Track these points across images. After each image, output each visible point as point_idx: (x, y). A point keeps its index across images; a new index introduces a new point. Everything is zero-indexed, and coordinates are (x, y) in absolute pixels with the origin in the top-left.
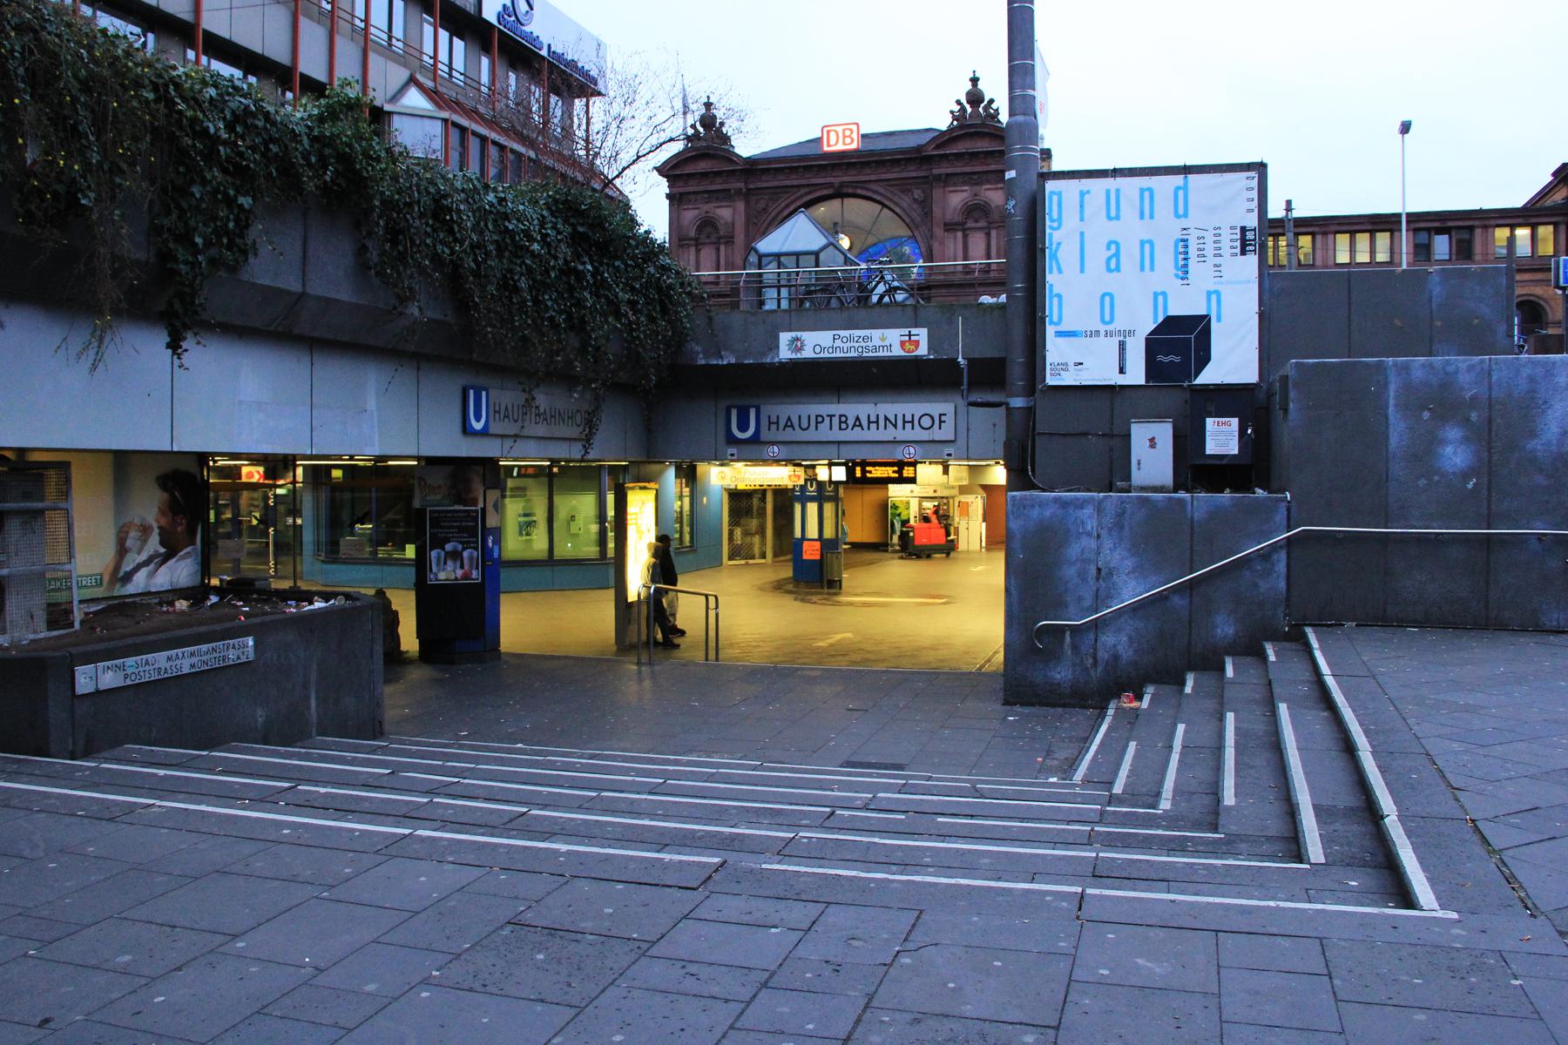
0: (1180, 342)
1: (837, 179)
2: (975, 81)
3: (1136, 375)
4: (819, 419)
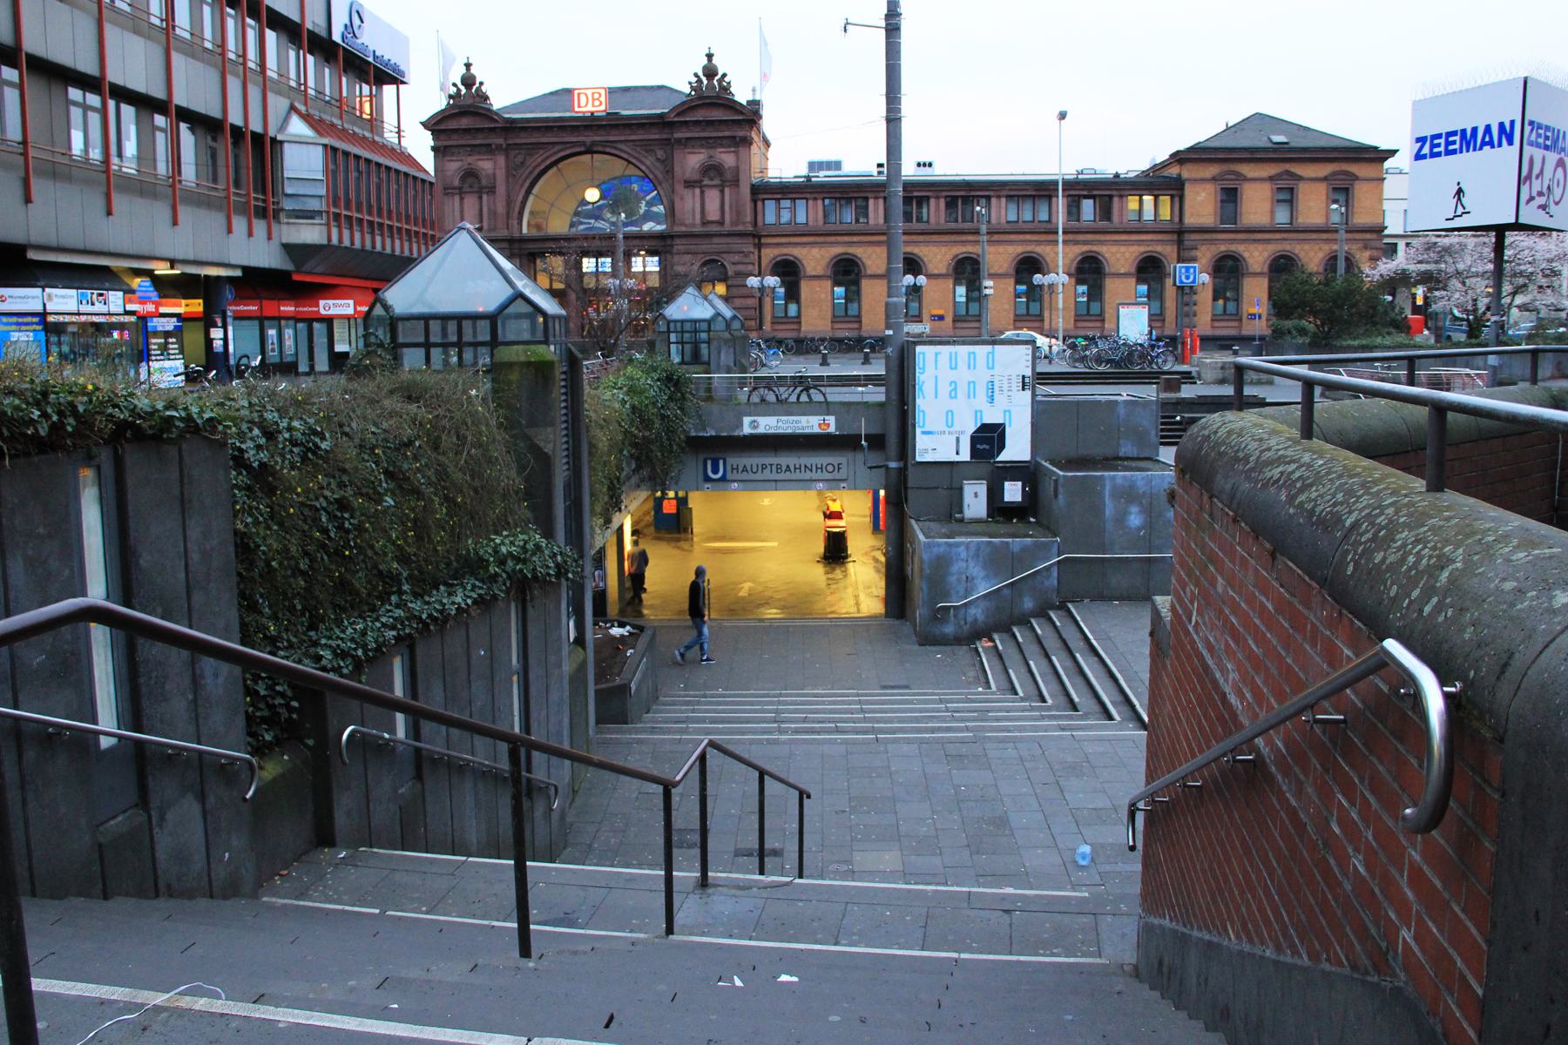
0: (989, 437)
1: (589, 138)
2: (710, 56)
3: (965, 456)
4: (764, 467)
